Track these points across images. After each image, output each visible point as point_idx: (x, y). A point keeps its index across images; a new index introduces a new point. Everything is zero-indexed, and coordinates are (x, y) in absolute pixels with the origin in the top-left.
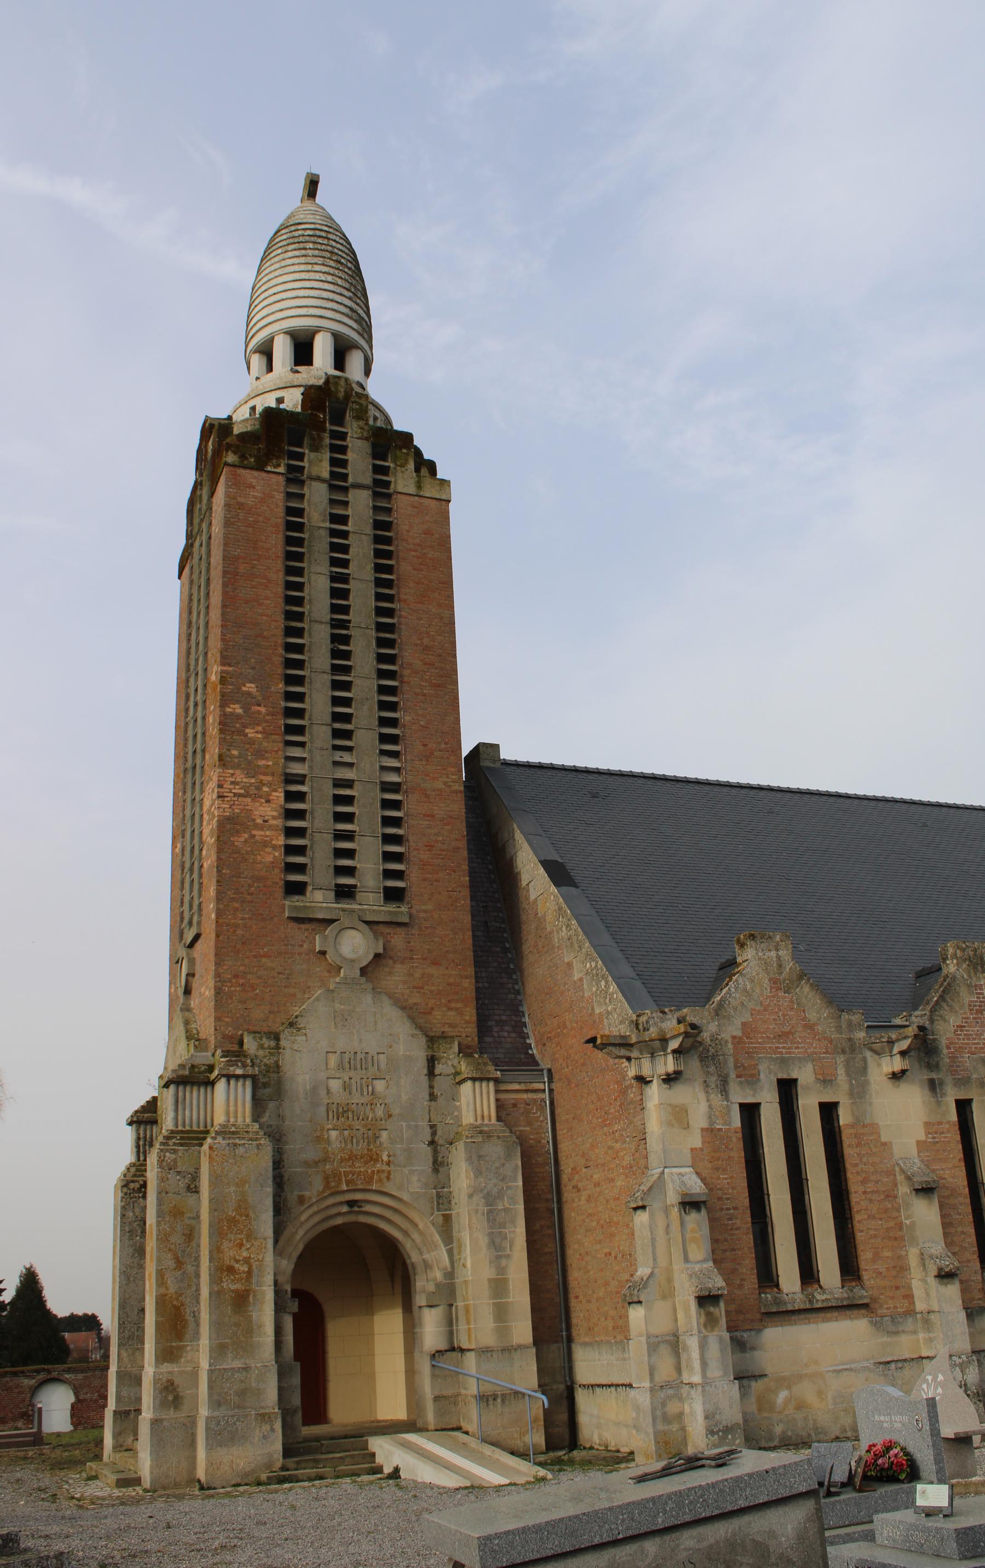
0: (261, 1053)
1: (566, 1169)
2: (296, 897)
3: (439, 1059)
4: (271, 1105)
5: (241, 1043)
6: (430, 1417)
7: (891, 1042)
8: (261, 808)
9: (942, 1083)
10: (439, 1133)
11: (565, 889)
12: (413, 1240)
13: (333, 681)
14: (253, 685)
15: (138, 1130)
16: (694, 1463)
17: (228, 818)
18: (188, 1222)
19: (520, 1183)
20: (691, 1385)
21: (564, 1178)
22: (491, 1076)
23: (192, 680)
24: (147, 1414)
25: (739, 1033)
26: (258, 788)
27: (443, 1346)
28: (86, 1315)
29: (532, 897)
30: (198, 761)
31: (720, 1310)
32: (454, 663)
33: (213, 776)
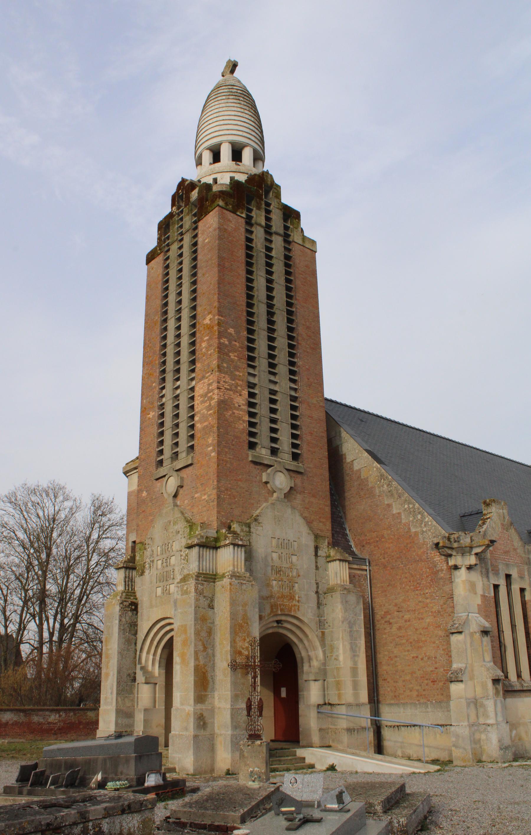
8: (237, 398)
10: (320, 587)
14: (233, 330)
15: (125, 572)
18: (209, 625)
19: (363, 618)
26: (236, 387)
27: (322, 702)
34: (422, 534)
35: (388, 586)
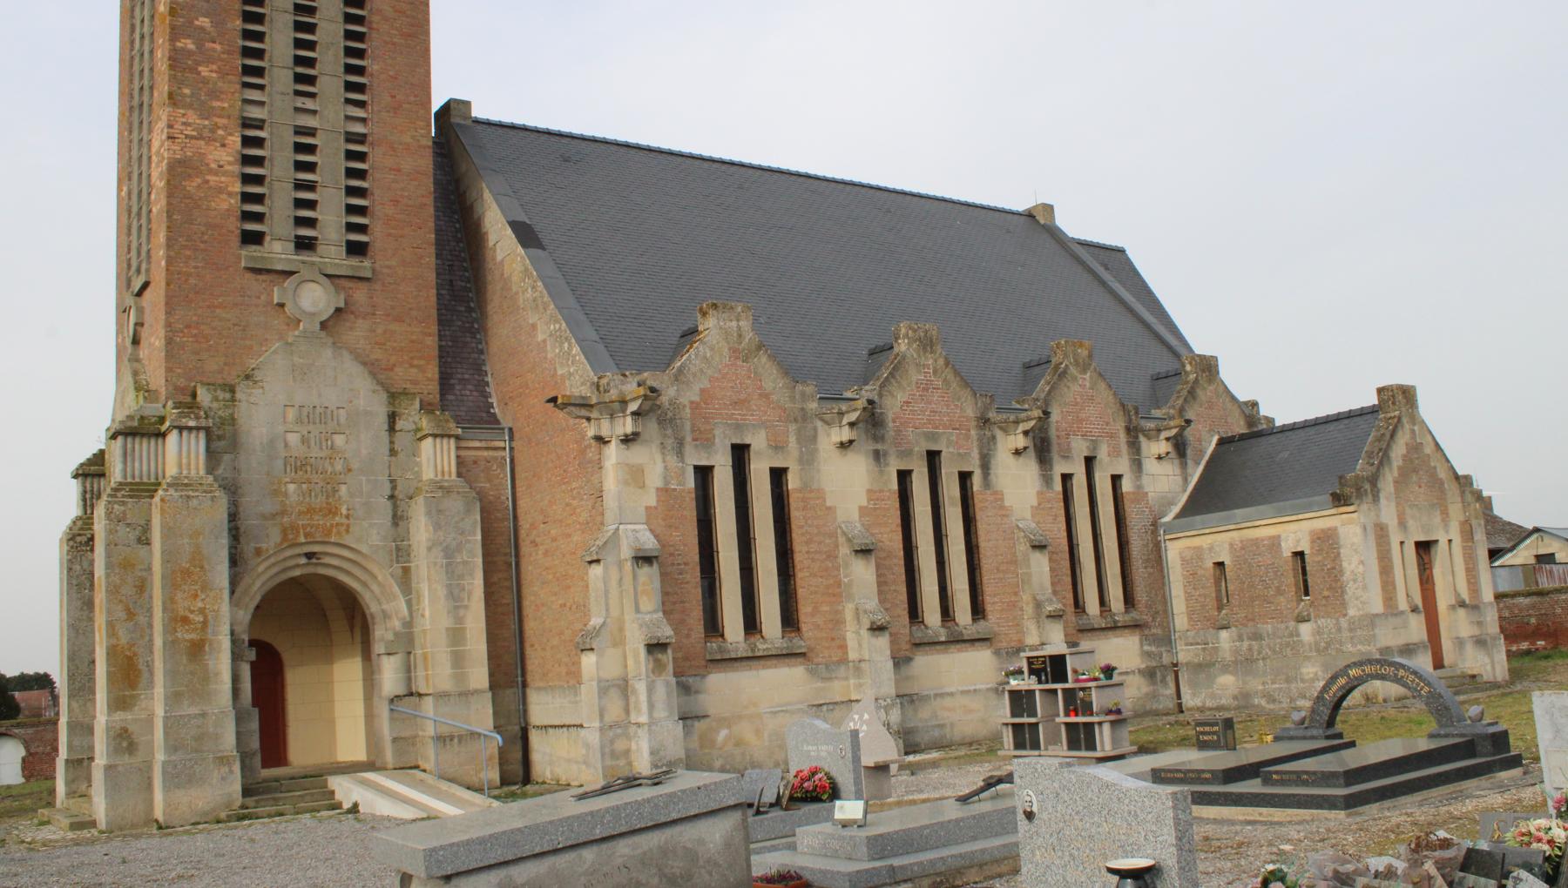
0: (215, 405)
1: (524, 524)
2: (254, 247)
3: (400, 415)
5: (194, 395)
6: (389, 757)
7: (841, 414)
9: (885, 454)
11: (533, 251)
13: (296, 22)
16: (632, 782)
17: (179, 162)
19: (479, 537)
20: (638, 725)
21: (523, 534)
23: (138, 10)
24: (100, 760)
25: (696, 398)
26: (213, 131)
27: (401, 691)
28: (37, 674)
29: (499, 258)
30: (146, 99)
31: (668, 657)
32: (427, 13)
33: (162, 115)
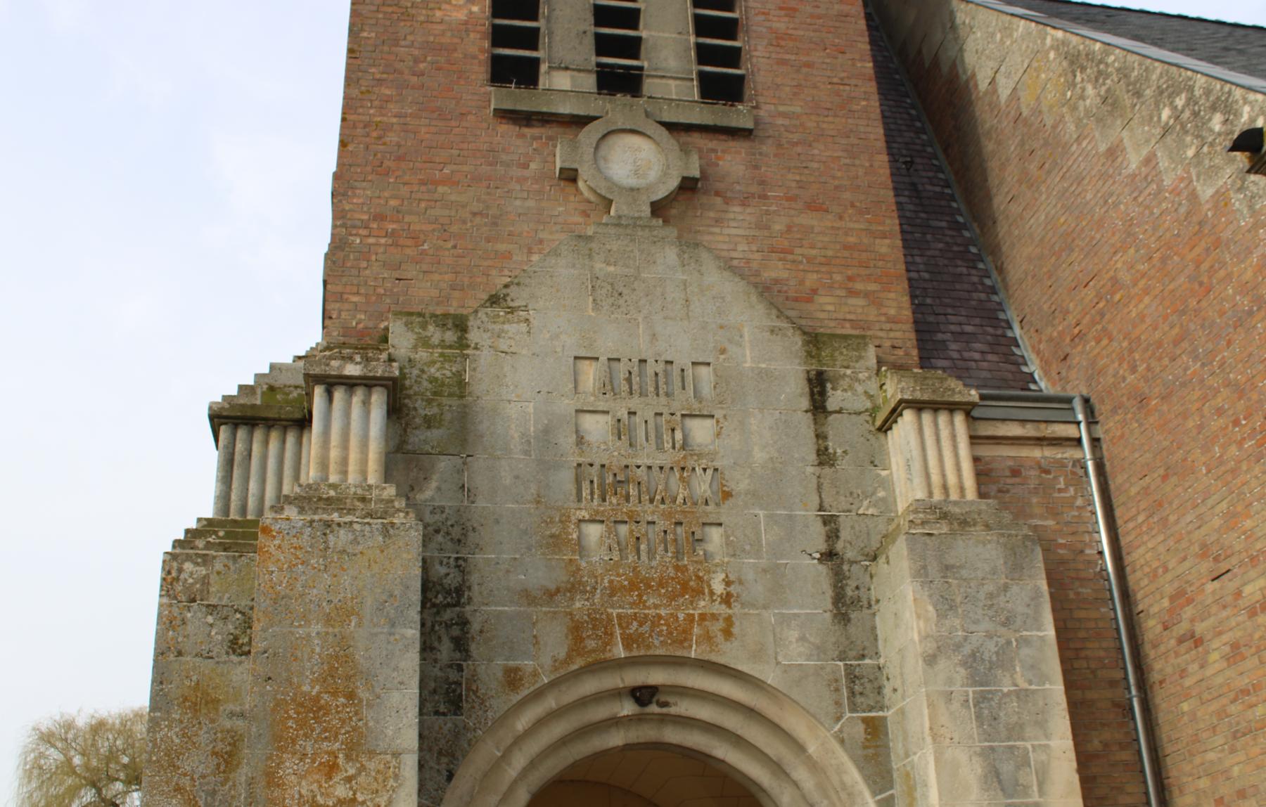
0: (422, 355)
3: (835, 381)
4: (444, 464)
10: (845, 534)
12: (796, 784)
18: (228, 724)
19: (1051, 632)
21: (1151, 627)
22: (957, 398)
34: (1240, 190)
35: (1165, 478)
